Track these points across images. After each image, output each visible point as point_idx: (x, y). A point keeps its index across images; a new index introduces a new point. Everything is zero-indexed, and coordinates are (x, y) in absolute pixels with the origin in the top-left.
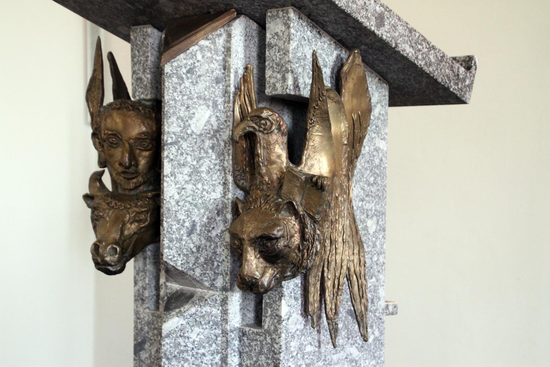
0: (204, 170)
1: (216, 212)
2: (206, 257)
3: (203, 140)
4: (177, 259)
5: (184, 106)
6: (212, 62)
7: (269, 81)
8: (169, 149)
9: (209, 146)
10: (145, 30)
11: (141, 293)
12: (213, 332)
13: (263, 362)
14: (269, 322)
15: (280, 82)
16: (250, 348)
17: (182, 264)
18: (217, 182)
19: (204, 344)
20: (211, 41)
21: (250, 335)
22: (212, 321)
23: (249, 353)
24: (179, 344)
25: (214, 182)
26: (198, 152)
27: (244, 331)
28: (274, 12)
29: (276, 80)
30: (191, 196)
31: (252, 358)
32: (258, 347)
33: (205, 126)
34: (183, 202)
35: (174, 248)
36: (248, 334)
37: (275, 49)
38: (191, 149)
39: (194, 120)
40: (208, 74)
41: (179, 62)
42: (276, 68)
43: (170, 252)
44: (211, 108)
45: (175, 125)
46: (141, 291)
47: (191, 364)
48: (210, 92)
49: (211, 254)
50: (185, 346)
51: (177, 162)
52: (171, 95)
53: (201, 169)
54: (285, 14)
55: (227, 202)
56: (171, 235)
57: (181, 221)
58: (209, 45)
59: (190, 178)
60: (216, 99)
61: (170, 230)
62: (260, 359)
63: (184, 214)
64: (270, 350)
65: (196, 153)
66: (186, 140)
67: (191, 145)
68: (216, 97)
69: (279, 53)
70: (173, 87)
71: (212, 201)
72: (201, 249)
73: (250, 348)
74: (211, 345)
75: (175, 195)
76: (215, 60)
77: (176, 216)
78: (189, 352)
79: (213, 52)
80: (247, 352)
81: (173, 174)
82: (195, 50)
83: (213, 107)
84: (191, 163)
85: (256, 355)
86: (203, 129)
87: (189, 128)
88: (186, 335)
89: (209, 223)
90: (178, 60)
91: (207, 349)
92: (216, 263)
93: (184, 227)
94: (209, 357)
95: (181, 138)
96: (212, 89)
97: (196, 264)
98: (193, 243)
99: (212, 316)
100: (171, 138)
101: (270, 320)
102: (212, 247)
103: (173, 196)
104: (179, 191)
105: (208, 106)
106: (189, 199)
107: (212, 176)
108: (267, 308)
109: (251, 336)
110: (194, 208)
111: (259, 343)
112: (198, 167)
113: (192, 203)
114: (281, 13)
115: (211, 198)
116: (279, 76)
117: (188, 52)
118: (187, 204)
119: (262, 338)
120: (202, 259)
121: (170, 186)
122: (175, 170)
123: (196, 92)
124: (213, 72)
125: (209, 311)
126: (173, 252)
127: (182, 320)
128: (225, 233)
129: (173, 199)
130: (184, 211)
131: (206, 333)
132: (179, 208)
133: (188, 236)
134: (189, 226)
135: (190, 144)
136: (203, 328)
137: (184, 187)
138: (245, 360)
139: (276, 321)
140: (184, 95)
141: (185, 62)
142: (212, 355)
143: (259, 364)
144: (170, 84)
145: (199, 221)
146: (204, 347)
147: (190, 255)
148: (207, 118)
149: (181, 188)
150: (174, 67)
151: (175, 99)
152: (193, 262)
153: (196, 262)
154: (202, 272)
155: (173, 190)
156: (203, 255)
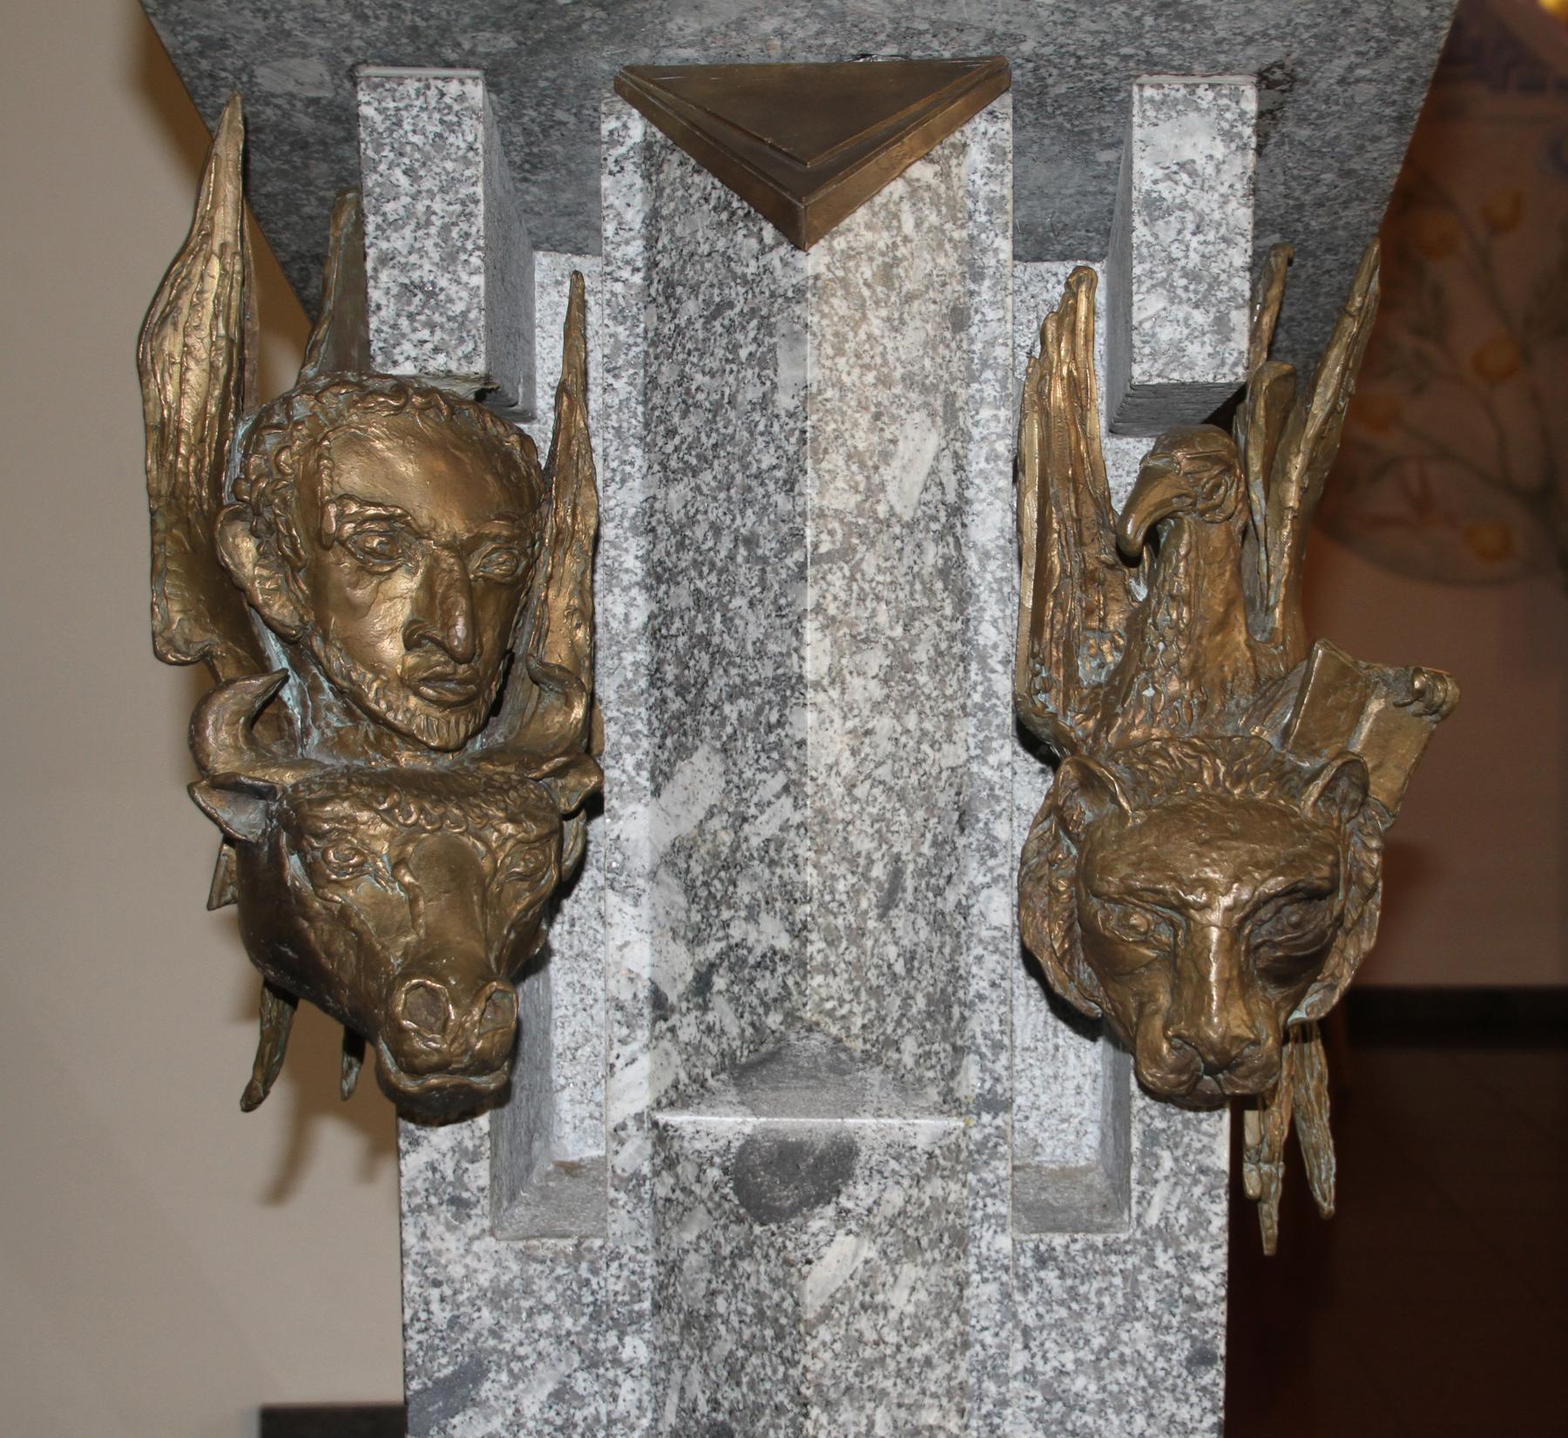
0: (924, 658)
1: (955, 816)
2: (931, 989)
3: (919, 546)
4: (851, 1012)
5: (866, 409)
6: (940, 245)
7: (1154, 335)
8: (823, 578)
9: (935, 566)
10: (453, 88)
11: (450, 1177)
12: (951, 1271)
13: (1141, 1347)
14: (1167, 1200)
15: (1206, 339)
16: (1075, 1306)
17: (864, 1027)
18: (956, 703)
19: (928, 1323)
20: (937, 168)
21: (1073, 1259)
22: (948, 1229)
23: (1071, 1325)
24: (860, 1339)
25: (949, 705)
26: (907, 588)
27: (1043, 1248)
28: (1175, 87)
29: (1186, 332)
30: (890, 762)
31: (1087, 1342)
32: (1113, 1296)
33: (926, 489)
34: (867, 784)
35: (843, 966)
36: (1061, 1257)
37: (1182, 220)
38: (889, 579)
39: (896, 463)
40: (931, 294)
41: (851, 237)
42: (1186, 289)
43: (828, 985)
44: (939, 421)
45: (840, 484)
46: (448, 1168)
47: (894, 1407)
48: (939, 360)
49: (943, 978)
50: (877, 1344)
51: (846, 630)
52: (828, 363)
53: (914, 657)
54: (1225, 101)
55: (996, 779)
56: (831, 918)
57: (862, 861)
58: (934, 182)
59: (886, 691)
60: (953, 388)
61: (828, 898)
62: (1124, 1336)
63: (870, 831)
64: (1169, 1302)
65: (901, 595)
66: (873, 544)
67: (888, 564)
68: (954, 380)
69: (1201, 238)
70: (836, 334)
71: (944, 775)
72: (916, 964)
73: (1075, 1306)
74: (946, 1323)
75: (843, 760)
76: (950, 240)
77: (846, 839)
78: (888, 1360)
79: (944, 210)
80: (1059, 1324)
81: (836, 677)
82: (896, 197)
83: (945, 421)
84: (889, 633)
85: (1103, 1328)
86: (919, 503)
87: (881, 496)
88: (879, 1298)
89: (937, 858)
90: (849, 230)
91: (938, 1338)
92: (956, 1011)
93: (868, 880)
94: (943, 1369)
95: (860, 536)
96: (941, 350)
97: (905, 1021)
98: (896, 943)
99: (948, 1213)
100: (831, 533)
101: (1173, 1191)
102: (947, 950)
103: (837, 763)
104: (855, 743)
105: (932, 415)
106: (884, 772)
107: (942, 681)
108: (1157, 1150)
109: (1082, 1261)
110: (898, 805)
111: (1118, 1281)
112: (907, 646)
113: (891, 789)
114: (1206, 97)
115: (944, 765)
116: (1199, 318)
117: (878, 200)
118: (877, 791)
119: (1132, 1261)
120: (920, 1002)
121: (827, 725)
122: (844, 661)
123: (898, 359)
124: (944, 284)
125: (940, 1193)
126: (838, 984)
127: (866, 1243)
128: (985, 893)
129: (838, 774)
130: (868, 822)
131: (933, 1280)
132: (856, 807)
133: (881, 917)
134: (883, 878)
135: (887, 560)
136: (924, 1264)
137: (870, 726)
138: (1049, 1355)
139: (1198, 1191)
140: (867, 367)
141: (869, 236)
142: (951, 1355)
143: (1122, 1355)
144: (825, 322)
145: (910, 857)
146: (929, 1335)
147: (887, 991)
148: (931, 462)
149: (861, 731)
150: (837, 256)
151: (839, 380)
152: (896, 1015)
153: (903, 1015)
154: (920, 1051)
155: (837, 739)
156: (924, 983)
